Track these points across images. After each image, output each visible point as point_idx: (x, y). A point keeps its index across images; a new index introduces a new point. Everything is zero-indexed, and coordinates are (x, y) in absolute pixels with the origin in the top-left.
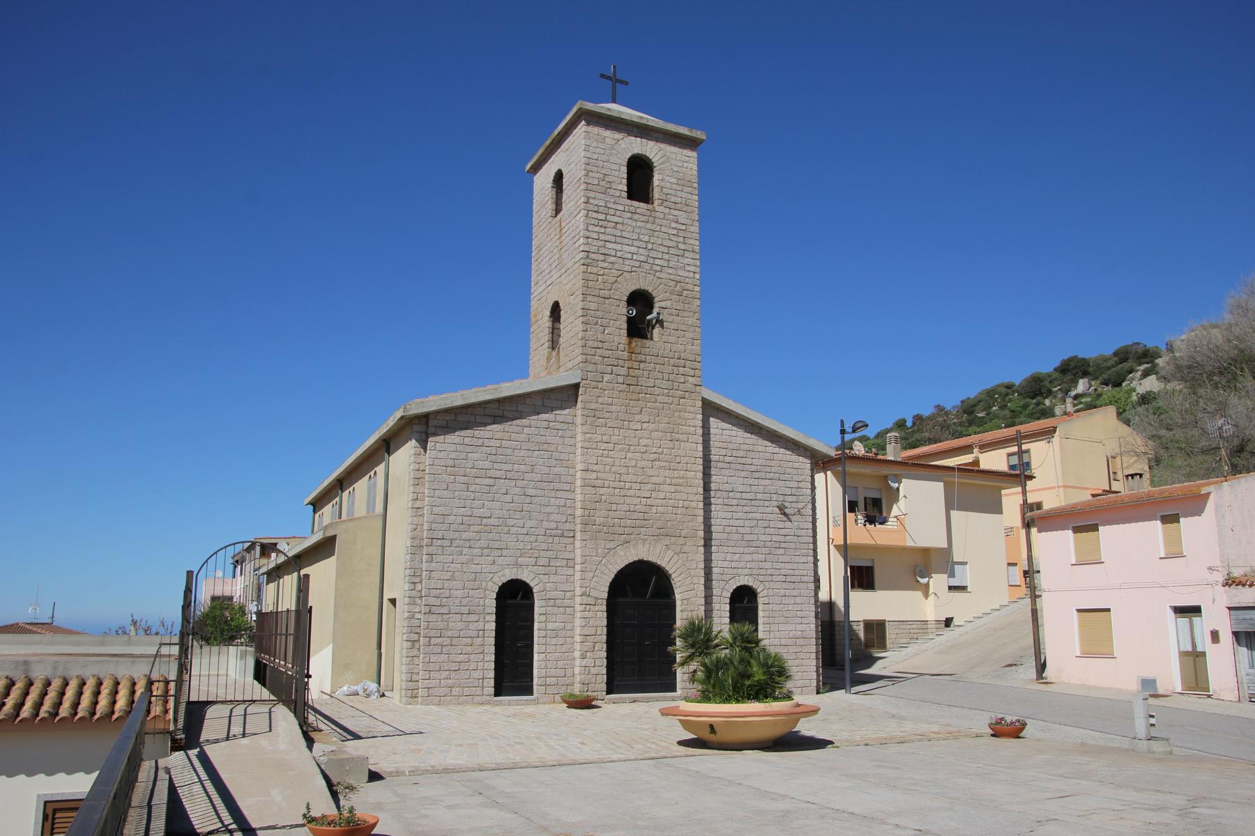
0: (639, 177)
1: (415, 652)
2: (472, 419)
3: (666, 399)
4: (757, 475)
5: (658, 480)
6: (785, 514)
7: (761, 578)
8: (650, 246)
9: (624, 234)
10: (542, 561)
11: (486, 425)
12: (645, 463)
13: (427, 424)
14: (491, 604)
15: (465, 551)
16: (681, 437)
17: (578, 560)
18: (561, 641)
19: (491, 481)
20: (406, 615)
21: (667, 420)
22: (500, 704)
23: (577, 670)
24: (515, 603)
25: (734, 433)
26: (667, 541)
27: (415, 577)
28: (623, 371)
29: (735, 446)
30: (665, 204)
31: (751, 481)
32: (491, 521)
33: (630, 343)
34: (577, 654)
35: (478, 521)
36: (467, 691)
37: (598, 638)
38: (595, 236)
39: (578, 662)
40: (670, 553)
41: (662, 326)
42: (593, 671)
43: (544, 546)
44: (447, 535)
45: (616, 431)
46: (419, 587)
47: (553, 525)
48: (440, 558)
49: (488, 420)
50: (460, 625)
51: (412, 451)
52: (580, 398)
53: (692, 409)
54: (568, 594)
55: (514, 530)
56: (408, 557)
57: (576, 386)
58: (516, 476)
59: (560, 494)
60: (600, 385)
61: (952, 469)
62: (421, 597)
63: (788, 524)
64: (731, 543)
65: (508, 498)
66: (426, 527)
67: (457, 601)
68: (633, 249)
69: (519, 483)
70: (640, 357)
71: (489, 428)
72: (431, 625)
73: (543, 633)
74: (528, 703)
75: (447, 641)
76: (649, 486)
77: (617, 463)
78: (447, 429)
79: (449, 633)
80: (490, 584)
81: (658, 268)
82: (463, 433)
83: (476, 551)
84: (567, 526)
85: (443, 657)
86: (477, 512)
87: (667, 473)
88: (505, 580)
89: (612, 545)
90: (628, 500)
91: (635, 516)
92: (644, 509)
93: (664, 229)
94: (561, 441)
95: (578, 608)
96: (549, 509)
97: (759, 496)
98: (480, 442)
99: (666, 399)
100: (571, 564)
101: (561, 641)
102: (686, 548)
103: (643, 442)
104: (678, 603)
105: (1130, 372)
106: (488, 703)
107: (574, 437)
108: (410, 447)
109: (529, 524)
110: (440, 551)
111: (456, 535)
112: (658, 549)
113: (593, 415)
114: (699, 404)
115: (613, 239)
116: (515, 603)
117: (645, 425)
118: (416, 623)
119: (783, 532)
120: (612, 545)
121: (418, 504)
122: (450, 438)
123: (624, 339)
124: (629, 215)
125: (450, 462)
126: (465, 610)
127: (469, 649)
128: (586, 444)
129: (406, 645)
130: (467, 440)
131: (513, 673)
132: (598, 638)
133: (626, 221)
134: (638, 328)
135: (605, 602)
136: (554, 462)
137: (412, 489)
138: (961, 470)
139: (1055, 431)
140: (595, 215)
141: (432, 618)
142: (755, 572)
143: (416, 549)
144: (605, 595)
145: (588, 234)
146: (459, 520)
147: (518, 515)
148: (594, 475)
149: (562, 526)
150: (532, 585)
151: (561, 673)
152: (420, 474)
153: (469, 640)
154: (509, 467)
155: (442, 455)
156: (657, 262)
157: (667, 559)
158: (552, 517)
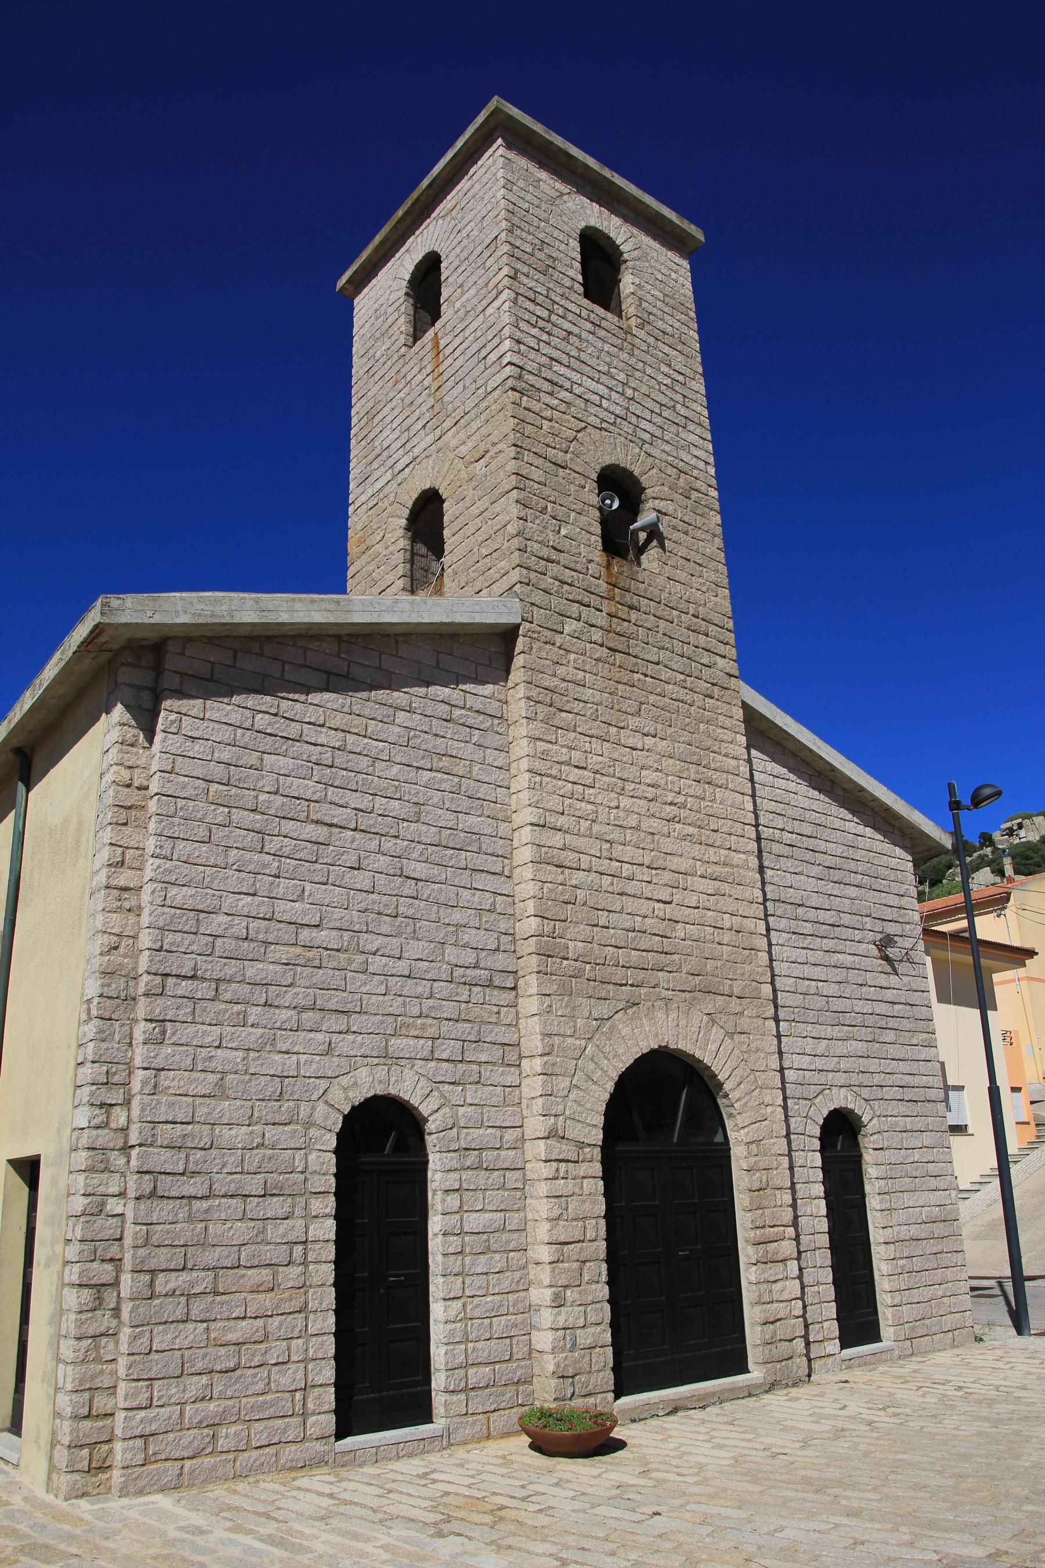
0: (600, 268)
1: (106, 1321)
2: (275, 669)
3: (682, 694)
4: (836, 875)
5: (683, 864)
6: (887, 959)
7: (865, 1093)
8: (629, 393)
9: (583, 356)
11: (308, 690)
12: (655, 824)
13: (158, 670)
14: (322, 1164)
15: (254, 1014)
16: (715, 775)
17: (533, 1043)
18: (498, 1261)
20: (79, 1203)
21: (686, 736)
22: (352, 1460)
23: (543, 1340)
25: (792, 786)
26: (710, 1004)
27: (108, 1089)
29: (796, 813)
30: (648, 328)
31: (829, 888)
32: (323, 936)
33: (608, 566)
34: (541, 1295)
35: (287, 933)
36: (260, 1432)
38: (533, 343)
39: (546, 1317)
40: (716, 1033)
41: (662, 546)
42: (584, 1338)
43: (449, 1009)
44: (205, 967)
45: (596, 745)
46: (120, 1117)
47: (470, 957)
48: (186, 1033)
50: (242, 1231)
51: (115, 735)
52: (518, 661)
53: (728, 723)
54: (510, 1136)
55: (377, 963)
56: (90, 1029)
57: (508, 635)
58: (382, 825)
59: (481, 881)
60: (559, 639)
61: (943, 934)
62: (126, 1148)
63: (894, 980)
64: (811, 1016)
65: (362, 879)
66: (146, 940)
67: (233, 1159)
69: (388, 844)
70: (628, 598)
71: (315, 698)
72: (159, 1233)
73: (455, 1242)
74: (425, 1446)
75: (204, 1281)
76: (667, 876)
77: (603, 817)
78: (215, 684)
79: (211, 1257)
80: (321, 1108)
81: (647, 437)
82: (252, 701)
83: (285, 1014)
84: (501, 961)
85: (193, 1332)
86: (285, 909)
87: (697, 850)
88: (358, 1096)
89: (603, 1009)
90: (631, 905)
91: (646, 942)
92: (662, 927)
93: (649, 370)
94: (478, 755)
95: (539, 1170)
96: (457, 916)
97: (846, 919)
98: (293, 730)
99: (682, 694)
100: (512, 1057)
101: (498, 1261)
102: (744, 1023)
103: (649, 776)
104: (737, 1152)
105: (950, 868)
106: (316, 1462)
107: (503, 749)
108: (112, 726)
109: (416, 949)
110: (184, 1013)
111: (231, 969)
112: (695, 1021)
113: (549, 702)
114: (739, 714)
115: (565, 359)
117: (649, 741)
118: (108, 1227)
119: (889, 995)
120: (603, 1009)
121: (124, 878)
122: (220, 709)
123: (598, 556)
124: (588, 326)
125: (218, 771)
126: (254, 1184)
127: (266, 1300)
128: (538, 765)
129: (72, 1298)
130: (262, 721)
131: (381, 1373)
133: (584, 335)
135: (597, 1153)
136: (465, 804)
137: (108, 835)
138: (955, 936)
139: (1008, 899)
141: (162, 1210)
142: (855, 1079)
143: (113, 1006)
144: (597, 1136)
145: (518, 335)
146: (239, 926)
148: (557, 840)
149: (487, 960)
150: (424, 1110)
151: (498, 1349)
152: (133, 797)
154: (365, 802)
155: (197, 749)
156: (644, 424)
157: (712, 1047)
158: (468, 936)
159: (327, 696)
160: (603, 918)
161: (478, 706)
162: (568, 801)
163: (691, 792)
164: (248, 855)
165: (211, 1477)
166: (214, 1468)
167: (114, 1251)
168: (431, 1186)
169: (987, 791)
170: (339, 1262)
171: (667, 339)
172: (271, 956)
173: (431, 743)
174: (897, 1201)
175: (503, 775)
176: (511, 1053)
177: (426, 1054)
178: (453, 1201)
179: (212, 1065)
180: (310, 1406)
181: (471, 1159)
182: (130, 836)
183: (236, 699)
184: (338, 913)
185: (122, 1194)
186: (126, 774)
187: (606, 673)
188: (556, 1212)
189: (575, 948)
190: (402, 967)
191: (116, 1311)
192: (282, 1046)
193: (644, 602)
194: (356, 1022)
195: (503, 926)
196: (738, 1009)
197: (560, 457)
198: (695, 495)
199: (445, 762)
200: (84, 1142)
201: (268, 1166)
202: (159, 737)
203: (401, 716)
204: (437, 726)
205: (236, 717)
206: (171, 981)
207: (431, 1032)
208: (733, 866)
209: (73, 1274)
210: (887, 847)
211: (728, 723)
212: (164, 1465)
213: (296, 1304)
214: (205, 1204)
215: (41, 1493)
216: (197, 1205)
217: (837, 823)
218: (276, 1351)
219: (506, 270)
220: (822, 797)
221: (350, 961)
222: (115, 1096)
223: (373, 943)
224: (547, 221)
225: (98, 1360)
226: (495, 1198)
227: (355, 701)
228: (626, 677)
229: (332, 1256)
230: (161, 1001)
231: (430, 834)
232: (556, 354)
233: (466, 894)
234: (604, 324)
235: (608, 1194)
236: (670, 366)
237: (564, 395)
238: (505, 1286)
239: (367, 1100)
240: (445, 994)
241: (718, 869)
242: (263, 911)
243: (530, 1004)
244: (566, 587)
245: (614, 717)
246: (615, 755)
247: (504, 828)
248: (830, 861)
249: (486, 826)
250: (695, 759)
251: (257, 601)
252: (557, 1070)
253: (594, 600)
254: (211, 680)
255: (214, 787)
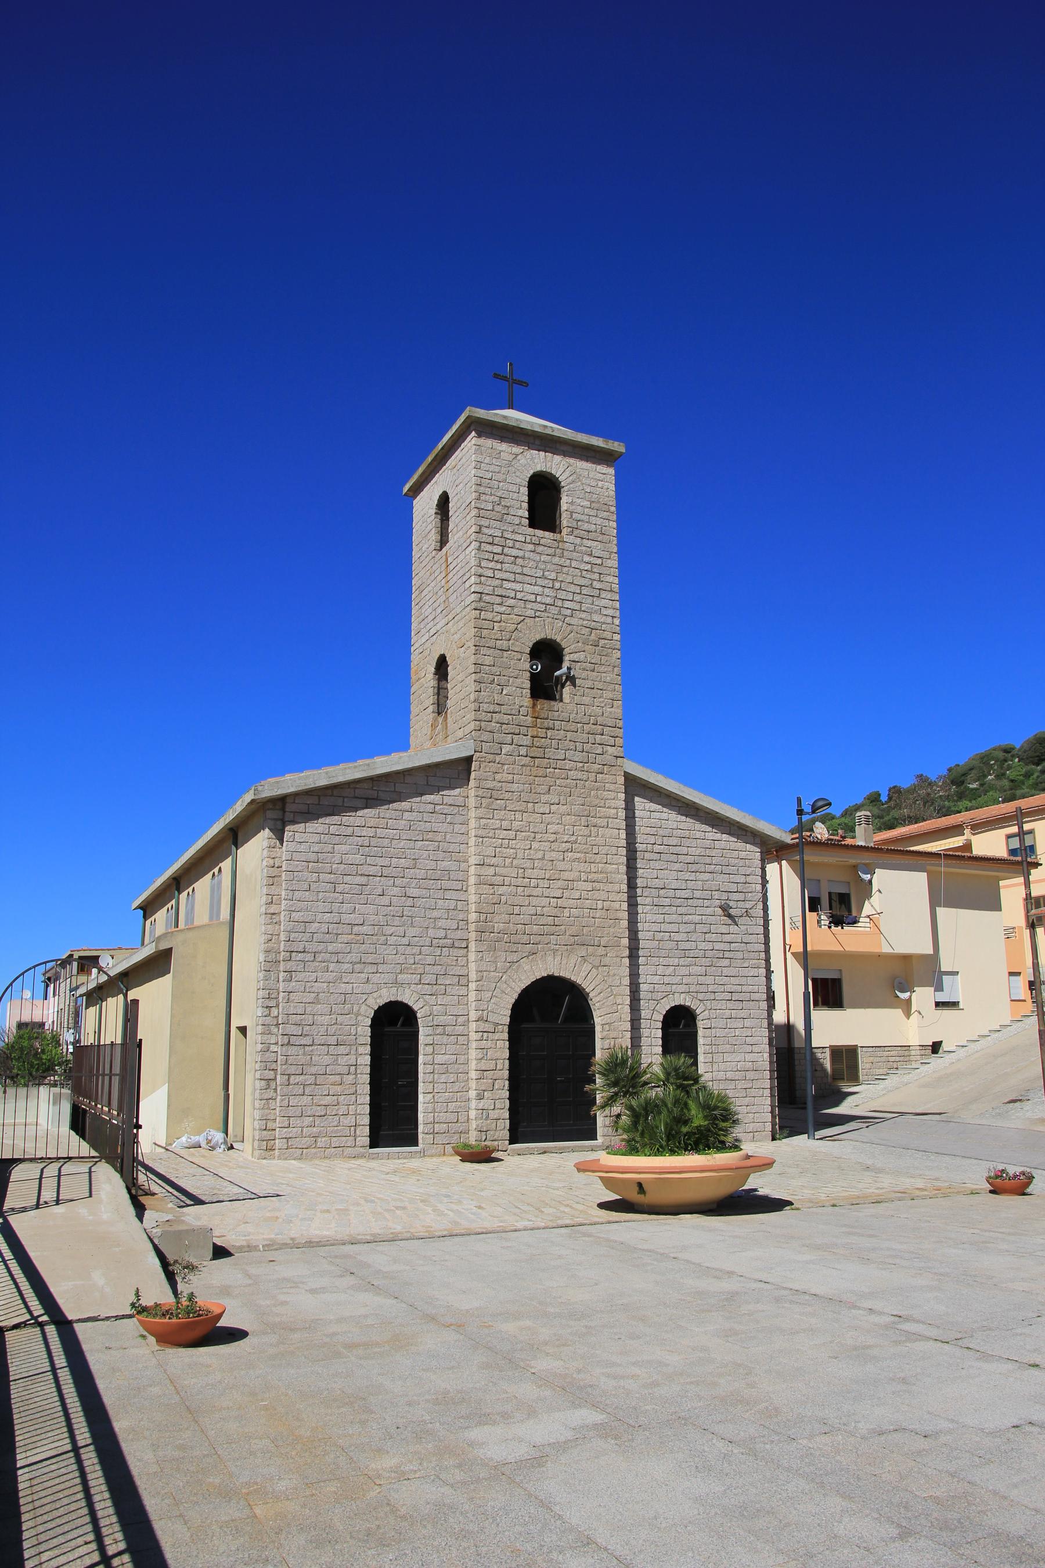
0: (543, 501)
1: (271, 1093)
2: (339, 802)
3: (580, 775)
4: (694, 867)
6: (730, 916)
7: (701, 996)
8: (557, 585)
9: (526, 571)
10: (427, 979)
11: (356, 809)
14: (365, 1032)
15: (332, 966)
18: (452, 1078)
19: (364, 880)
20: (259, 1047)
21: (580, 801)
23: (473, 1114)
24: (394, 1032)
25: (665, 816)
26: (582, 951)
27: (270, 1000)
28: (526, 741)
30: (576, 532)
31: (687, 876)
32: (364, 929)
33: (534, 706)
34: (472, 1094)
36: (335, 1142)
37: (498, 1074)
39: (473, 1104)
40: (587, 967)
42: (493, 1114)
43: (430, 960)
45: (518, 815)
46: (274, 1012)
47: (442, 933)
48: (301, 976)
49: (359, 803)
50: (327, 1060)
51: (266, 844)
52: (473, 775)
53: (612, 787)
54: (461, 1020)
55: (392, 940)
56: (261, 975)
57: (469, 760)
59: (449, 895)
62: (278, 1025)
63: (733, 928)
64: (663, 953)
65: (385, 900)
66: (283, 937)
67: (323, 1029)
68: (537, 589)
69: (398, 881)
70: (546, 723)
71: (360, 813)
72: (291, 1060)
73: (430, 1068)
75: (311, 1079)
76: (560, 883)
77: (520, 855)
79: (313, 1070)
80: (363, 1007)
82: (328, 820)
83: (346, 966)
84: (459, 934)
85: (306, 1100)
87: (583, 867)
89: (514, 957)
92: (555, 912)
95: (473, 1036)
96: (435, 914)
97: (697, 894)
99: (580, 775)
100: (463, 981)
101: (452, 1078)
102: (606, 960)
106: (362, 1156)
107: (465, 823)
109: (411, 932)
111: (321, 947)
112: (572, 961)
114: (621, 780)
116: (394, 1032)
119: (728, 938)
120: (514, 957)
122: (313, 826)
124: (531, 547)
125: (313, 857)
126: (332, 1040)
127: (339, 1089)
129: (259, 1084)
132: (498, 1074)
134: (545, 686)
136: (441, 855)
137: (265, 890)
140: (489, 548)
141: (292, 1050)
142: (693, 988)
143: (270, 965)
145: (480, 571)
147: (397, 921)
150: (415, 1008)
151: (453, 1117)
152: (275, 872)
153: (338, 1078)
155: (303, 847)
157: (584, 974)
159: (366, 811)
160: (517, 910)
161: (452, 802)
162: (498, 850)
163: (581, 833)
164: (328, 894)
165: (314, 1157)
166: (316, 1153)
167: (274, 1066)
168: (420, 1042)
169: (820, 803)
170: (372, 1074)
171: (592, 535)
172: (339, 940)
173: (422, 826)
174: (718, 1058)
175: (464, 837)
176: (462, 980)
177: (417, 981)
178: (429, 1049)
179: (313, 990)
180: (358, 1133)
181: (440, 1030)
182: (274, 890)
183: (320, 821)
184: (373, 917)
185: (276, 1043)
186: (271, 862)
187: (528, 773)
188: (480, 1056)
189: (498, 926)
190: (405, 941)
191: (275, 1090)
192: (344, 980)
193: (557, 723)
194: (381, 968)
195: (461, 917)
196: (604, 953)
197: (504, 644)
198: (602, 642)
199: (430, 836)
200: (260, 1022)
201: (338, 1032)
202: (285, 844)
203: (406, 815)
204: (426, 817)
205: (320, 829)
206: (294, 954)
207: (420, 971)
208: (606, 873)
209: (258, 1075)
210: (741, 845)
211: (612, 787)
212: (295, 1149)
213: (352, 1090)
214: (311, 1048)
215: (250, 1158)
216: (307, 1048)
217: (698, 835)
218: (343, 1110)
219: (474, 529)
220: (688, 819)
221: (378, 940)
222: (272, 1003)
223: (389, 930)
224: (505, 481)
225: (268, 1108)
226: (451, 1048)
227: (382, 811)
228: (541, 772)
229: (369, 1071)
230: (290, 963)
231: (421, 874)
232: (505, 576)
233: (440, 902)
234: (542, 541)
235: (511, 1048)
236: (591, 555)
237: (511, 602)
238: (456, 1089)
239: (386, 1004)
240: (428, 952)
241: (596, 876)
242: (335, 920)
243: (472, 956)
244: (504, 726)
245: (532, 797)
246: (531, 820)
247: (463, 865)
248: (689, 859)
249: (453, 866)
250: (586, 813)
251: (327, 773)
252: (484, 988)
253: (523, 730)
254: (308, 813)
255: (311, 864)
